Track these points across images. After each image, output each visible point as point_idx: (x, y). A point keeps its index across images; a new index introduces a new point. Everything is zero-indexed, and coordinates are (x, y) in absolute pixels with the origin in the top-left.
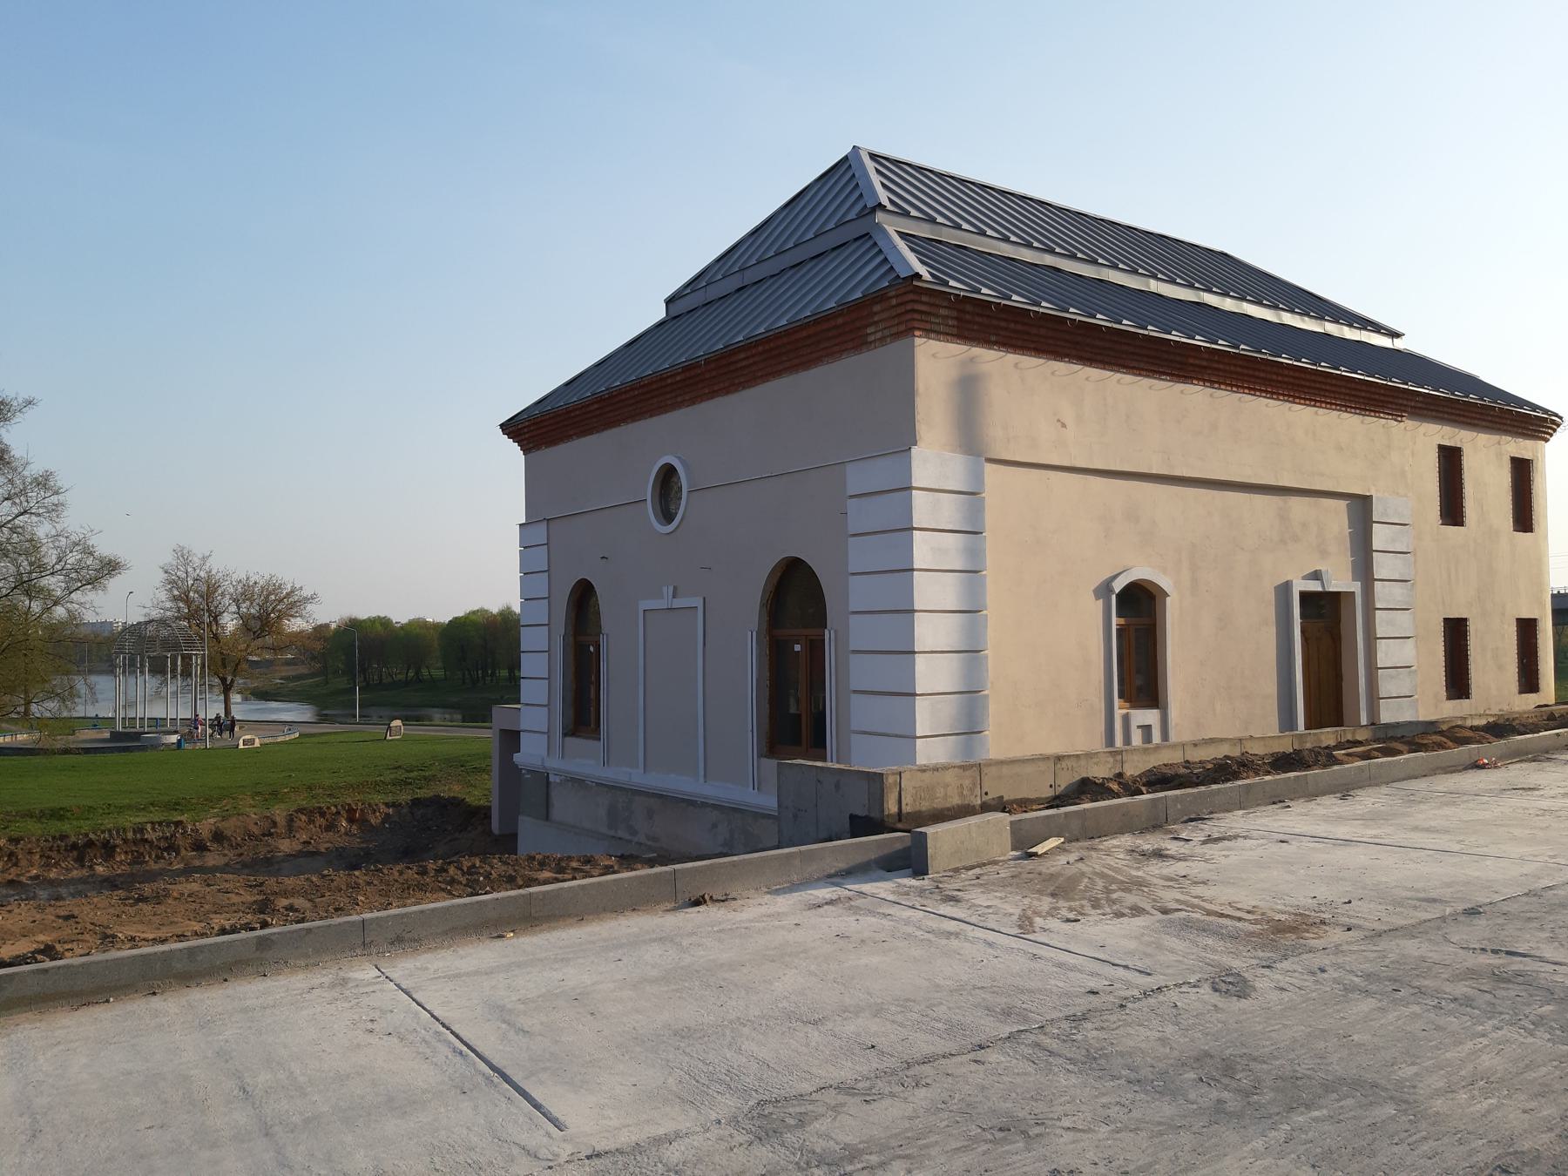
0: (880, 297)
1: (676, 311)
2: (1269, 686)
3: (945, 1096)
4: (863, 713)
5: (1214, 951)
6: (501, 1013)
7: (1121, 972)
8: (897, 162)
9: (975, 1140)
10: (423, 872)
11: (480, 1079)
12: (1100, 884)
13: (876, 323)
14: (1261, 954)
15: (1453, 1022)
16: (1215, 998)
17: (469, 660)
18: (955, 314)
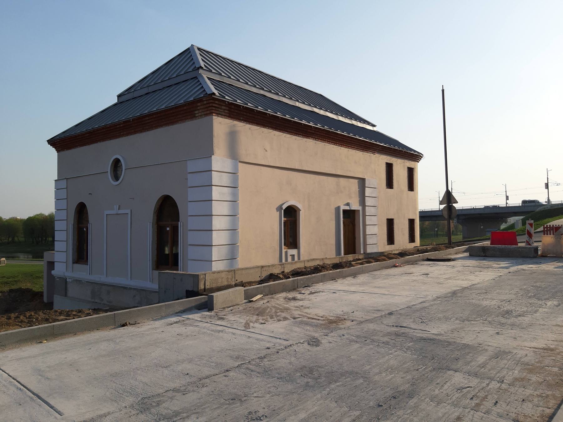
0: (200, 100)
1: (121, 100)
2: (333, 241)
3: (213, 389)
4: (192, 253)
5: (310, 331)
6: (39, 372)
7: (278, 340)
8: (208, 52)
9: (223, 404)
10: (9, 318)
11: (28, 399)
12: (274, 310)
13: (198, 110)
14: (324, 331)
15: (382, 350)
16: (309, 347)
17: (34, 234)
18: (228, 108)
